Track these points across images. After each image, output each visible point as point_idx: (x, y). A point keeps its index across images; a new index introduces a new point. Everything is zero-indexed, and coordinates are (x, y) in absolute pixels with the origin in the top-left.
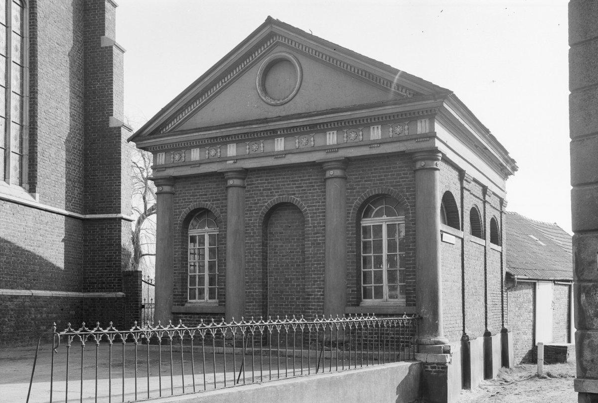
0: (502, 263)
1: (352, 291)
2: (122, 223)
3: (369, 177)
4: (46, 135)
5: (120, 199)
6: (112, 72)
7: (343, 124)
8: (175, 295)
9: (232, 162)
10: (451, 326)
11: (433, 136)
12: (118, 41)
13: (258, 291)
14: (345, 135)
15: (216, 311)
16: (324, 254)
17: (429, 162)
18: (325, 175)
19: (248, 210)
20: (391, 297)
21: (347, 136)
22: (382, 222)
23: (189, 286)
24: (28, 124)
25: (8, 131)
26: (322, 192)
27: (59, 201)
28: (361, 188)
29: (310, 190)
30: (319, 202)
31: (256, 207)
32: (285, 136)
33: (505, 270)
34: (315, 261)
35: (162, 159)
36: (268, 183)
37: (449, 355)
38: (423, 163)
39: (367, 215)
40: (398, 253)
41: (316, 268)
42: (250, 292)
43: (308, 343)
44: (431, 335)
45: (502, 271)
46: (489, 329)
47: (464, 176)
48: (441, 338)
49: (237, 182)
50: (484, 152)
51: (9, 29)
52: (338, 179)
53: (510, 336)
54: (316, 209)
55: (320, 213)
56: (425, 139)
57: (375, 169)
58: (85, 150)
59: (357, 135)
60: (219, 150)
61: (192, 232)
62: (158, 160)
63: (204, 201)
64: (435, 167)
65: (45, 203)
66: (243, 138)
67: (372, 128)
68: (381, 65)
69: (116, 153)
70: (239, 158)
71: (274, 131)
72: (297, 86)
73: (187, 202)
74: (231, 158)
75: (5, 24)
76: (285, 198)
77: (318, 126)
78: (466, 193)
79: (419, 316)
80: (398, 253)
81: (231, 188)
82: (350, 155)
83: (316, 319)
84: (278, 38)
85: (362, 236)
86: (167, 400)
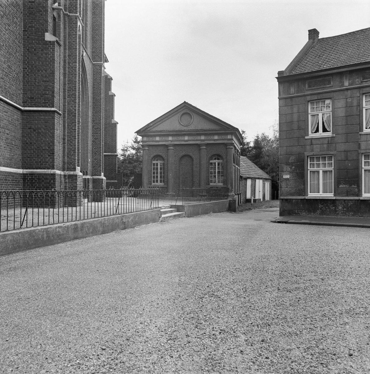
15: (163, 186)
23: (309, 168)
49: (204, 147)
74: (170, 141)
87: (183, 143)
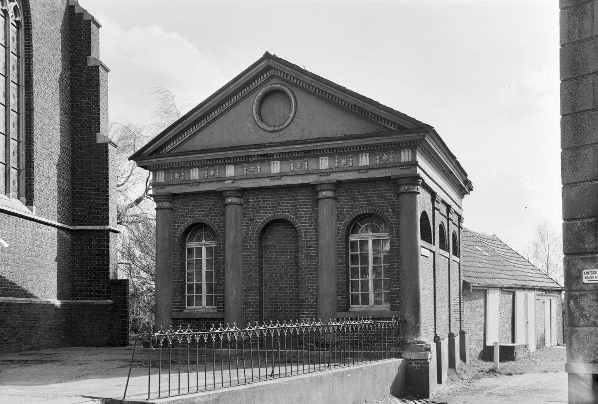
0: (460, 272)
1: (343, 298)
2: (110, 234)
3: (358, 198)
4: (40, 150)
5: (108, 211)
6: (99, 91)
7: (335, 151)
8: (174, 302)
9: (230, 181)
10: (427, 328)
11: (415, 164)
12: (102, 59)
13: (255, 298)
14: (337, 160)
15: (215, 316)
16: (317, 265)
17: (411, 187)
18: (317, 195)
19: (245, 226)
20: (376, 302)
21: (338, 162)
22: (368, 238)
24: (24, 141)
25: (8, 147)
26: (314, 210)
27: (51, 213)
28: (350, 208)
29: (304, 208)
30: (312, 220)
31: (253, 223)
32: (281, 160)
33: (463, 278)
34: (308, 271)
35: (161, 177)
36: (264, 201)
37: (429, 352)
38: (406, 188)
39: (355, 231)
40: (382, 265)
41: (308, 277)
42: (247, 299)
43: (302, 344)
44: (414, 335)
45: (460, 279)
46: (452, 331)
47: (436, 197)
48: (422, 338)
49: (235, 200)
50: (449, 175)
51: (8, 50)
52: (330, 199)
53: (467, 337)
54: (308, 226)
55: (312, 229)
56: (408, 167)
57: (363, 192)
58: (73, 164)
59: (348, 161)
60: (217, 171)
61: (189, 245)
62: (157, 178)
63: (202, 216)
64: (416, 191)
65: (41, 215)
66: (238, 160)
67: (360, 155)
68: (370, 101)
69: (104, 168)
70: (237, 178)
71: (272, 155)
72: (291, 115)
73: (185, 217)
74: (229, 178)
75: (4, 45)
76: (280, 216)
77: (312, 152)
78: (436, 212)
79: (404, 319)
80: (382, 265)
81: (229, 206)
82: (341, 179)
83: (212, 329)
84: (274, 71)
85: (350, 250)
86: (165, 400)
87: (267, 183)
